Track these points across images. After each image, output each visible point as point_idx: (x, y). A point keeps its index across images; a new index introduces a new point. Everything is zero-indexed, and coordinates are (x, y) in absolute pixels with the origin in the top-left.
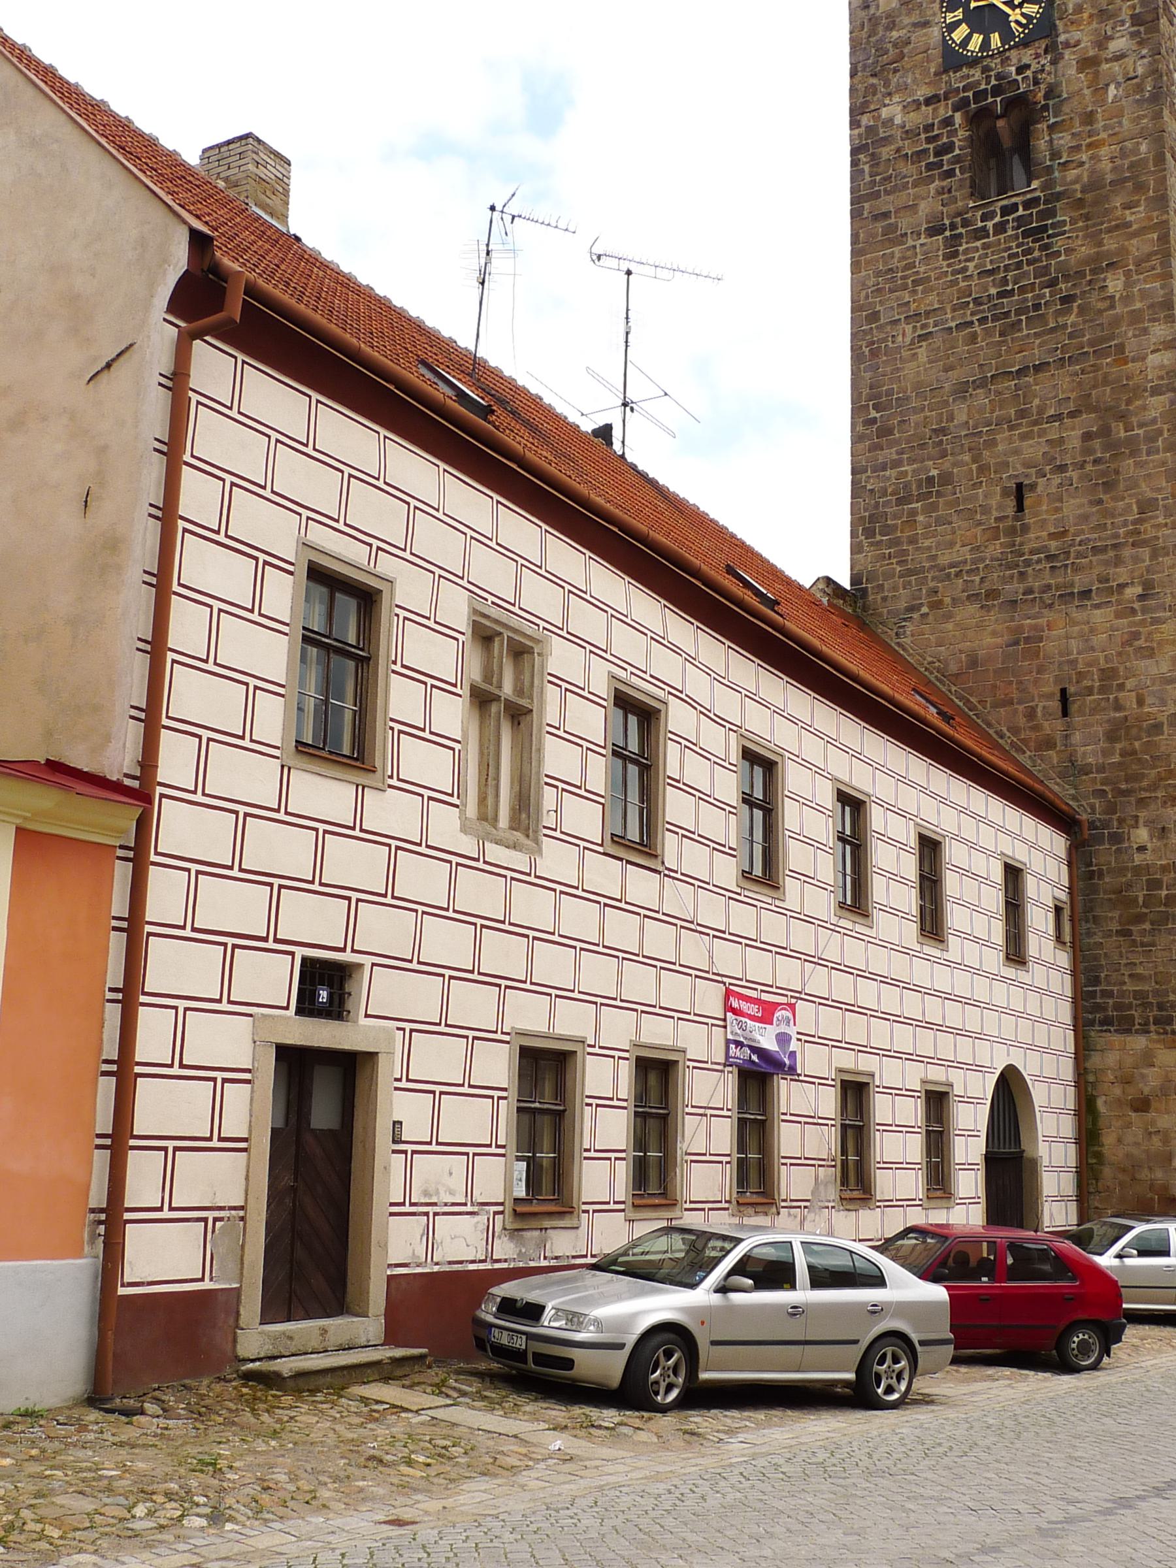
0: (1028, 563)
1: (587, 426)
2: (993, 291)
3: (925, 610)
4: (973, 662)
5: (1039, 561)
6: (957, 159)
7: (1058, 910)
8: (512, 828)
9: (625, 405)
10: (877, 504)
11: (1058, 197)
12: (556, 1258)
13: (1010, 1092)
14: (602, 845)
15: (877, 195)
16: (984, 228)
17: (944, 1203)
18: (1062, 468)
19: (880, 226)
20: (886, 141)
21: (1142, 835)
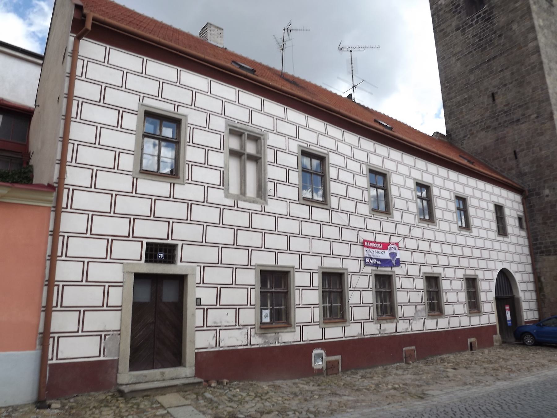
0: (498, 116)
1: (345, 96)
2: (477, 40)
3: (469, 136)
4: (485, 148)
5: (502, 114)
6: (462, 8)
7: (520, 219)
8: (257, 197)
9: (353, 87)
10: (451, 110)
11: (493, 7)
12: (284, 343)
13: (505, 278)
14: (298, 201)
15: (440, 25)
16: (472, 24)
17: (478, 314)
18: (505, 85)
19: (442, 33)
20: (441, 10)
21: (547, 192)
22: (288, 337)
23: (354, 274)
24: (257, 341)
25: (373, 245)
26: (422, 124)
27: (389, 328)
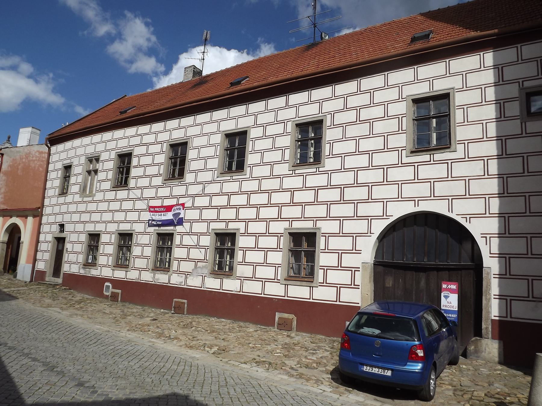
13: (64, 191)
22: (94, 272)
23: (140, 233)
24: (82, 272)
25: (157, 209)
26: (9, 138)
27: (162, 278)
